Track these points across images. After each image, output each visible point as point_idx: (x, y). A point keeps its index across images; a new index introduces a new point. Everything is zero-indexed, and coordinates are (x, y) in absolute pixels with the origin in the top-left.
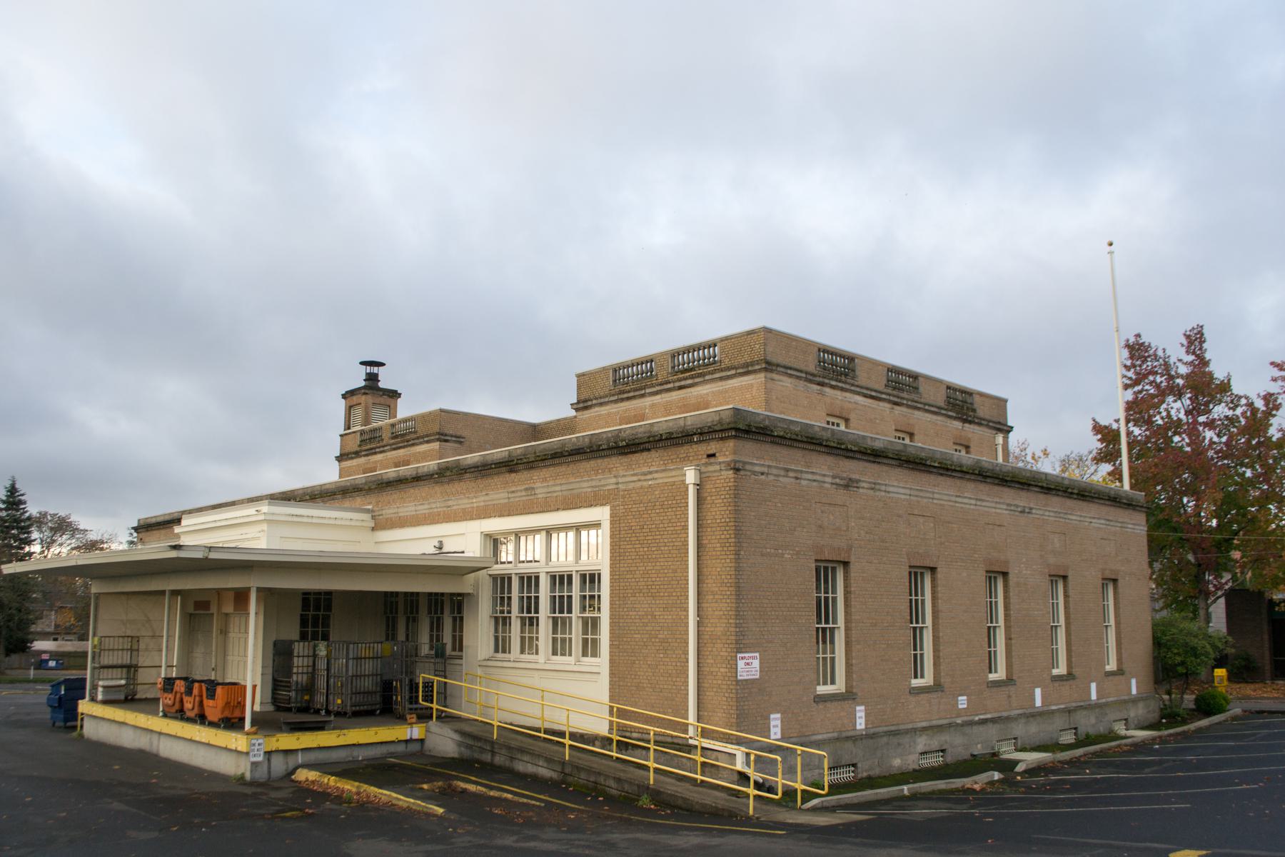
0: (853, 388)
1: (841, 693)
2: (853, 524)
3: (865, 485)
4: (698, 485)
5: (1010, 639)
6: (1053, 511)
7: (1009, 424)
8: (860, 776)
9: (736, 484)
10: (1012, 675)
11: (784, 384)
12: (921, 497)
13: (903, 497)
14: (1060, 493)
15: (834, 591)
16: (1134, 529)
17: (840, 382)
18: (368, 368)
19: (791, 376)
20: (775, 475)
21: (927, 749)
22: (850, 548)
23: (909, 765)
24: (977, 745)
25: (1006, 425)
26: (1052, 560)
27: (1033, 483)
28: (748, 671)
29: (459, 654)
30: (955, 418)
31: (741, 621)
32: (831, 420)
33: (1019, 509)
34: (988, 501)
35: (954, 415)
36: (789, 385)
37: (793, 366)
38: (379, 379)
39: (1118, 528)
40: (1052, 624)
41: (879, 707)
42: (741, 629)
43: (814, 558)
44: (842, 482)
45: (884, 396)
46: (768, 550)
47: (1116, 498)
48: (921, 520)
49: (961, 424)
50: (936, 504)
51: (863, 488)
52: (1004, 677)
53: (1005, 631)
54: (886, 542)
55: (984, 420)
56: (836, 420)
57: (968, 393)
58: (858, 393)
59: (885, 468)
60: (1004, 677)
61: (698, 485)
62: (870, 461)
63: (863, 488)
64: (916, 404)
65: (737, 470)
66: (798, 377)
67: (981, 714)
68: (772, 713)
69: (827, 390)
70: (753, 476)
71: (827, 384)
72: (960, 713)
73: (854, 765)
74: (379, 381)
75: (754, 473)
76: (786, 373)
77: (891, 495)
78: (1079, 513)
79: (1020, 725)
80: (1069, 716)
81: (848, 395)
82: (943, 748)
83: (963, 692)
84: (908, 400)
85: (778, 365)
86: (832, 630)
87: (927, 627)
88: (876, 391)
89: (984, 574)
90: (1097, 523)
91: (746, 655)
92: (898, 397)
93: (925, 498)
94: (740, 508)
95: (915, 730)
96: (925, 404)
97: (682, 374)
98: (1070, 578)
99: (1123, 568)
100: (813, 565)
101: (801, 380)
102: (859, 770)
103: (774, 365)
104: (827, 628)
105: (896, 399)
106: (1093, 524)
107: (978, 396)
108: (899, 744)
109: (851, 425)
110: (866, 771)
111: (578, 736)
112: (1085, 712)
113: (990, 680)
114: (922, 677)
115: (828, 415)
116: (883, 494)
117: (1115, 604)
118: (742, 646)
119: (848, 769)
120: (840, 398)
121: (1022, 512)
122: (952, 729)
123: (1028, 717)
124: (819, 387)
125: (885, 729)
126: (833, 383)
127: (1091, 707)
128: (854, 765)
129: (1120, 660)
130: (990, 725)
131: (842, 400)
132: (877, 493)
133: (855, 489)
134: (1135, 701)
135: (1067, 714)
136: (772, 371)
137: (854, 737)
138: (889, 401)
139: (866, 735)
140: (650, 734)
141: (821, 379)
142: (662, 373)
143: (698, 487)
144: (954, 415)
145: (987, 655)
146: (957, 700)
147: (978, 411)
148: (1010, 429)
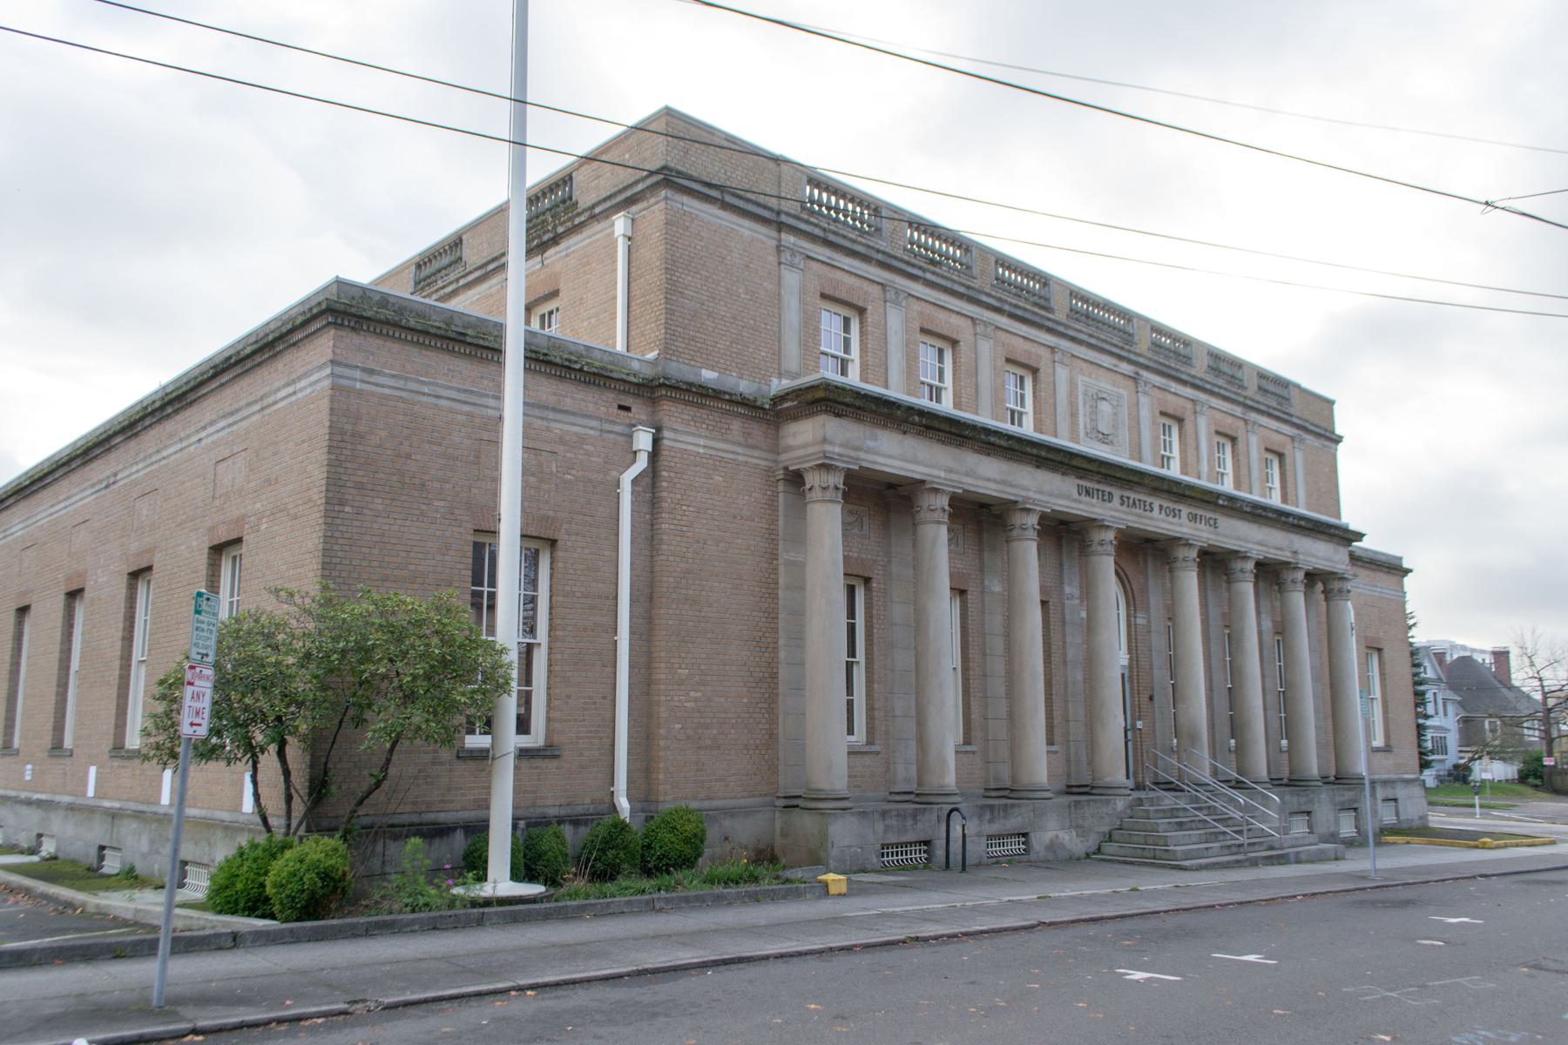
57: (1284, 384)
119: (913, 848)
135: (110, 820)
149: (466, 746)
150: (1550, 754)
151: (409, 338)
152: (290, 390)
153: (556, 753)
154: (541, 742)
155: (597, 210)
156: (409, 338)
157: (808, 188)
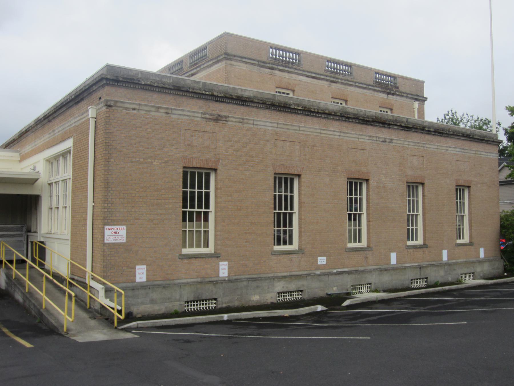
0: (297, 71)
1: (295, 250)
2: (221, 145)
3: (234, 120)
4: (95, 118)
5: (369, 221)
6: (440, 146)
7: (425, 96)
8: (220, 306)
9: (107, 115)
10: (370, 244)
11: (242, 68)
12: (287, 129)
13: (270, 128)
14: (419, 131)
15: (417, 197)
16: (487, 155)
17: (286, 67)
19: (246, 63)
20: (146, 111)
21: (285, 290)
22: (218, 160)
23: (267, 300)
24: (332, 288)
25: (424, 97)
26: (410, 172)
27: (392, 123)
28: (115, 237)
30: (381, 92)
31: (109, 205)
32: (383, 109)
33: (381, 140)
34: (351, 134)
35: (380, 89)
36: (246, 69)
37: (246, 56)
39: (472, 155)
40: (408, 213)
41: (241, 262)
42: (109, 210)
43: (182, 166)
44: (211, 117)
45: (322, 77)
46: (137, 159)
47: (470, 135)
48: (288, 144)
49: (386, 95)
50: (302, 134)
51: (232, 121)
52: (297, 248)
53: (367, 216)
54: (253, 157)
55: (404, 93)
56: (385, 110)
58: (302, 75)
59: (254, 110)
60: (297, 248)
61: (95, 118)
62: (239, 105)
63: (232, 121)
64: (348, 82)
65: (109, 106)
66: (252, 64)
67: (339, 268)
68: (138, 265)
69: (277, 72)
70: (124, 111)
71: (276, 68)
72: (319, 267)
73: (215, 299)
75: (126, 109)
76: (242, 61)
77: (259, 127)
78: (436, 144)
79: (374, 276)
80: (420, 271)
81: (294, 76)
82: (301, 289)
83: (323, 254)
84: (342, 79)
85: (235, 56)
86: (416, 215)
87: (419, 214)
88: (315, 73)
89: (346, 179)
90: (452, 151)
91: (114, 227)
92: (334, 78)
93: (291, 129)
94: (111, 131)
95: (274, 278)
96: (356, 82)
97: (193, 66)
98: (426, 184)
99: (476, 180)
100: (181, 171)
101: (254, 66)
102: (219, 303)
103: (231, 55)
104: (409, 214)
105: (332, 79)
106: (449, 151)
107: (401, 79)
108: (258, 287)
109: (296, 94)
110: (225, 303)
112: (435, 269)
113: (348, 247)
114: (463, 238)
115: (277, 87)
116: (252, 126)
117: (469, 202)
118: (109, 221)
120: (287, 77)
121: (385, 141)
122: (309, 278)
123: (381, 271)
124: (270, 70)
125: (247, 277)
126: (281, 68)
127: (442, 265)
128: (215, 299)
129: (471, 236)
130: (346, 276)
131: (288, 79)
132: (246, 125)
133: (224, 122)
134: (481, 262)
135: (419, 269)
136: (230, 60)
137: (215, 281)
138: (327, 80)
139: (228, 280)
141: (271, 65)
143: (96, 120)
144: (380, 89)
145: (406, 232)
146: (317, 259)
147: (400, 88)
148: (425, 99)
149: (145, 267)
150: (288, 169)
151: (150, 89)
152: (322, 131)
153: (218, 256)
154: (213, 252)
155: (409, 96)
156: (157, 90)
157: (327, 63)
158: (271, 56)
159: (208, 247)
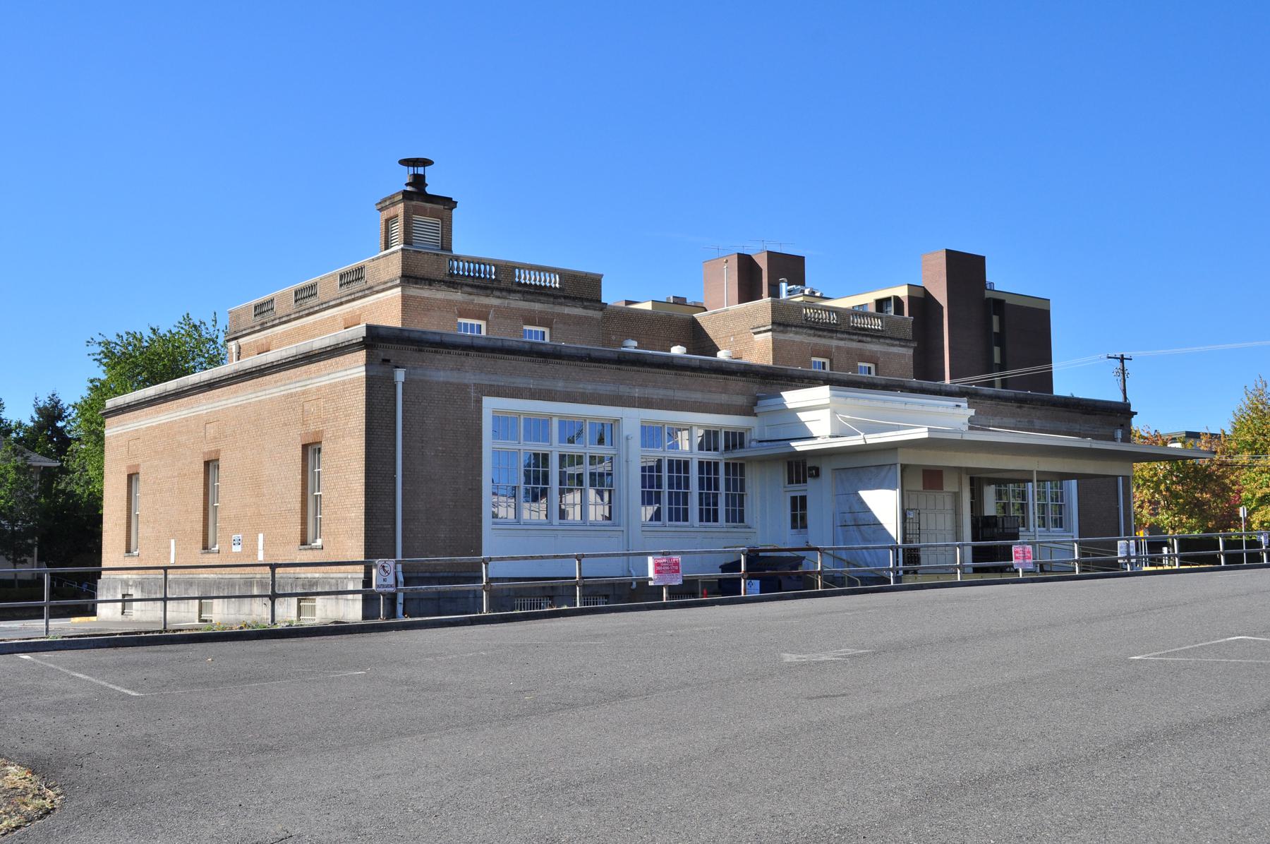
18: (411, 168)
29: (644, 424)
38: (426, 182)
74: (427, 185)
111: (100, 512)
140: (319, 491)
142: (880, 388)
158: (517, 280)
159: (687, 520)
